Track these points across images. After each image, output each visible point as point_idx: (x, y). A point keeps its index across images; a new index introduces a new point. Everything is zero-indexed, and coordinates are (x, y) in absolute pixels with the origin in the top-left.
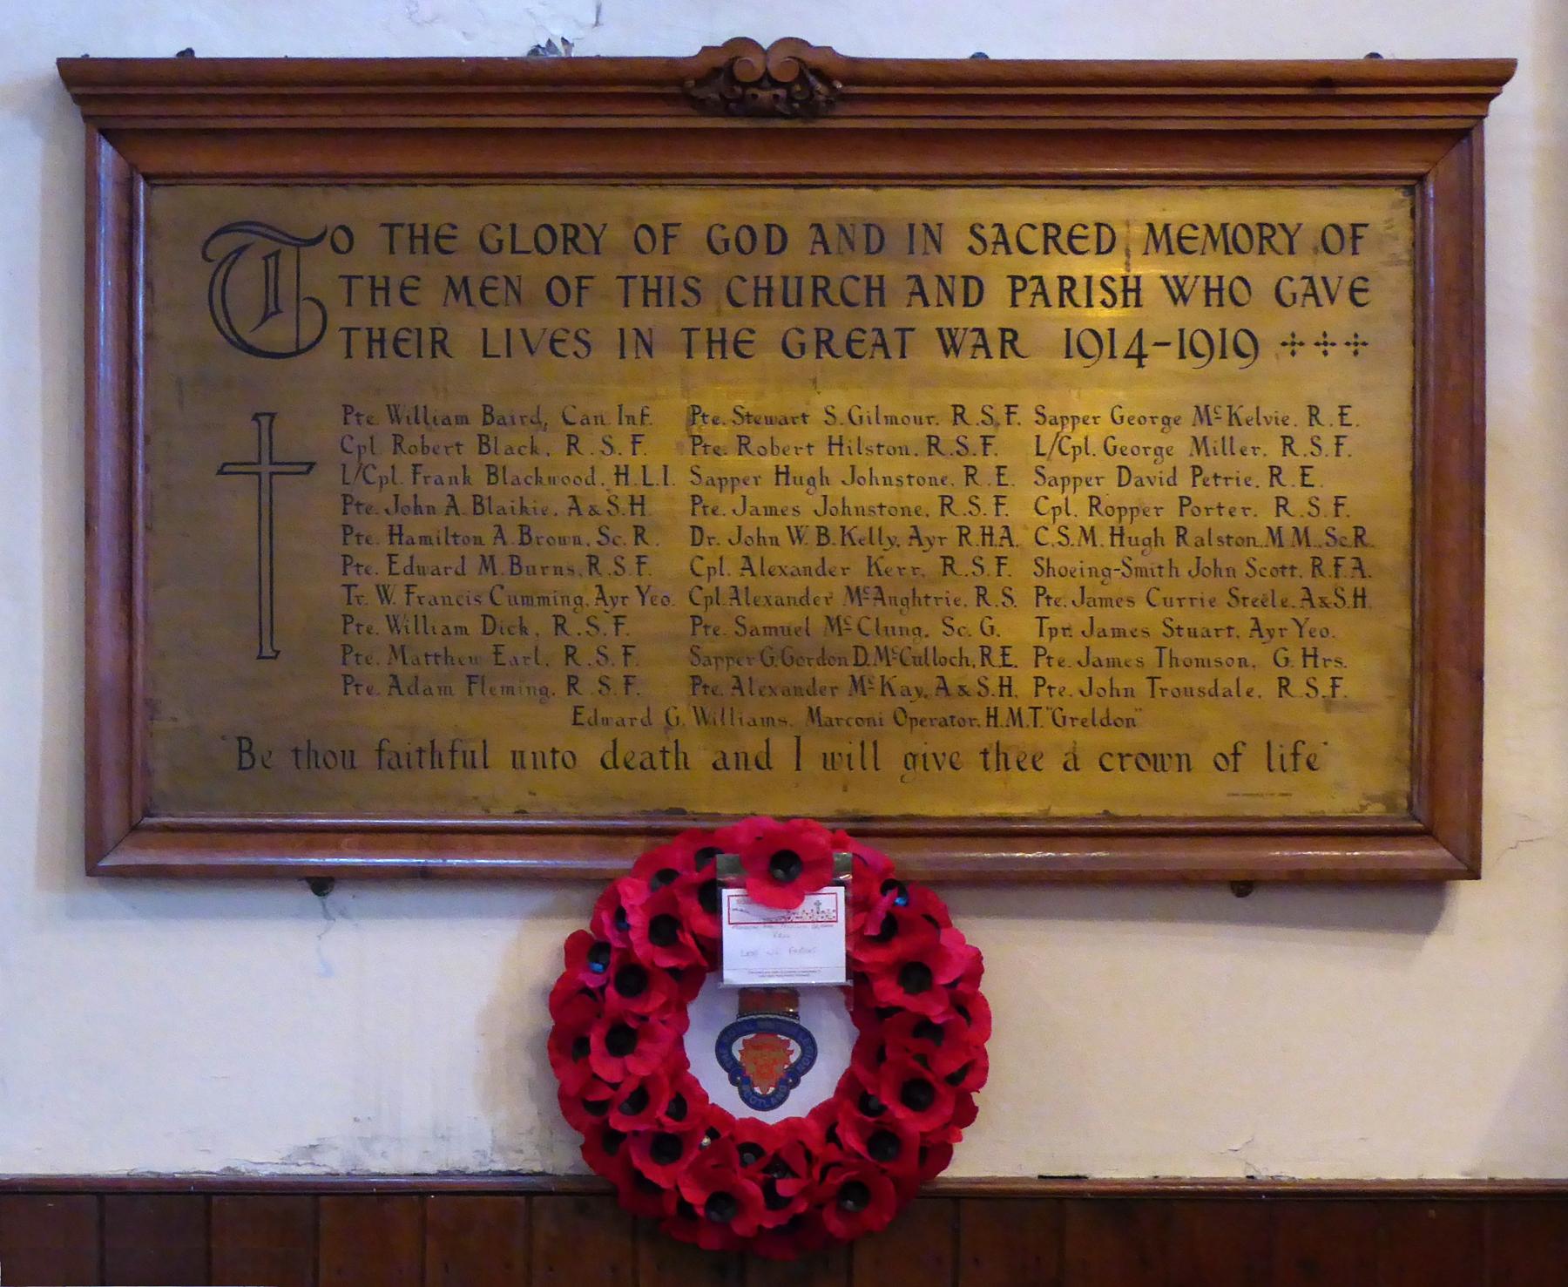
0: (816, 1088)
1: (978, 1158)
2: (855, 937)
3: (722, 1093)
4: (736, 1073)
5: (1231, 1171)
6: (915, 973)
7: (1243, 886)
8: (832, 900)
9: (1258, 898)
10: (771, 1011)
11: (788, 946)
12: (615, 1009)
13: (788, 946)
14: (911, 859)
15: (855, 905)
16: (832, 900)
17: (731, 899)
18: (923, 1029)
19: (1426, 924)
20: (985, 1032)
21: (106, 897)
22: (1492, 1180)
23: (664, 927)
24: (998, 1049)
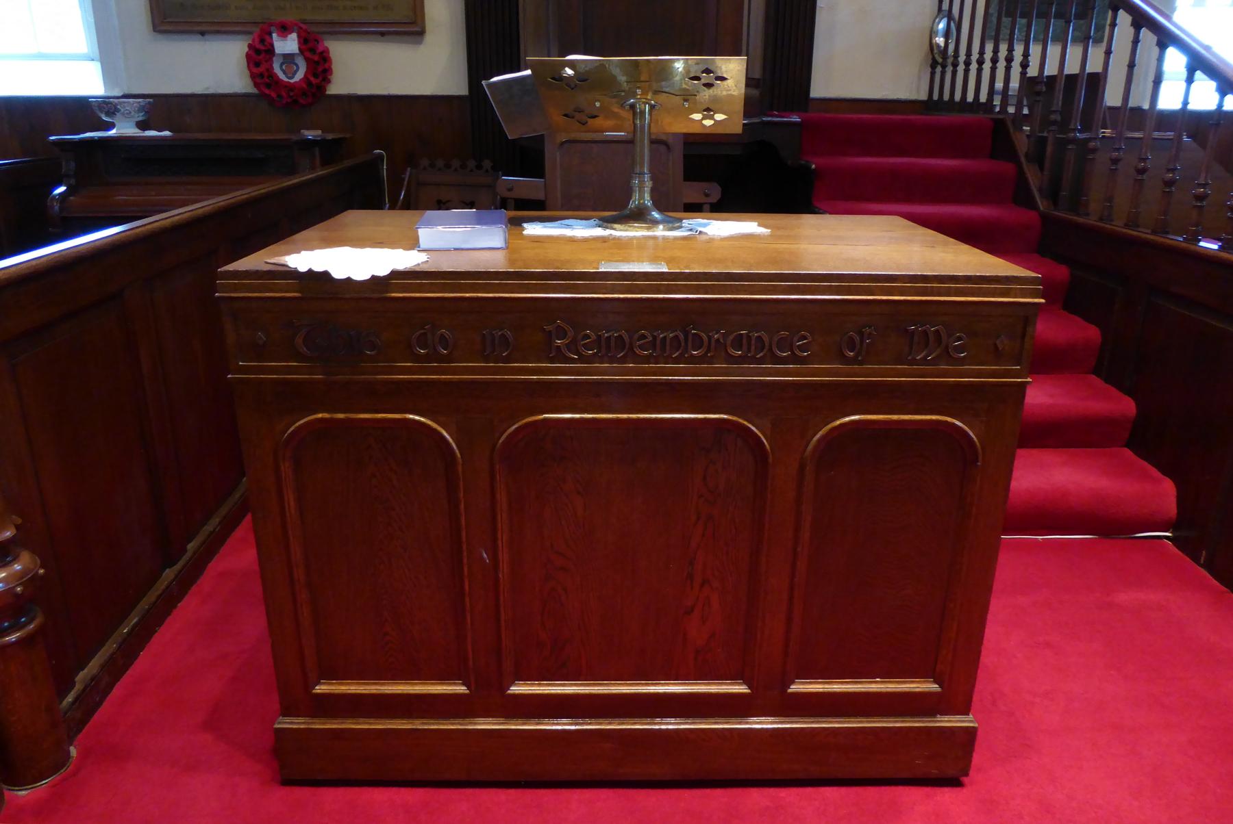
0: (299, 76)
1: (334, 89)
2: (299, 43)
3: (282, 76)
4: (284, 73)
5: (385, 93)
6: (313, 50)
7: (383, 34)
8: (294, 36)
9: (386, 37)
10: (288, 58)
11: (287, 45)
12: (259, 57)
13: (287, 45)
14: (314, 29)
15: (299, 37)
16: (294, 36)
17: (274, 35)
18: (320, 66)
19: (420, 43)
20: (405, 249)
21: (160, 36)
22: (1207, 48)
23: (262, 41)
24: (334, 67)
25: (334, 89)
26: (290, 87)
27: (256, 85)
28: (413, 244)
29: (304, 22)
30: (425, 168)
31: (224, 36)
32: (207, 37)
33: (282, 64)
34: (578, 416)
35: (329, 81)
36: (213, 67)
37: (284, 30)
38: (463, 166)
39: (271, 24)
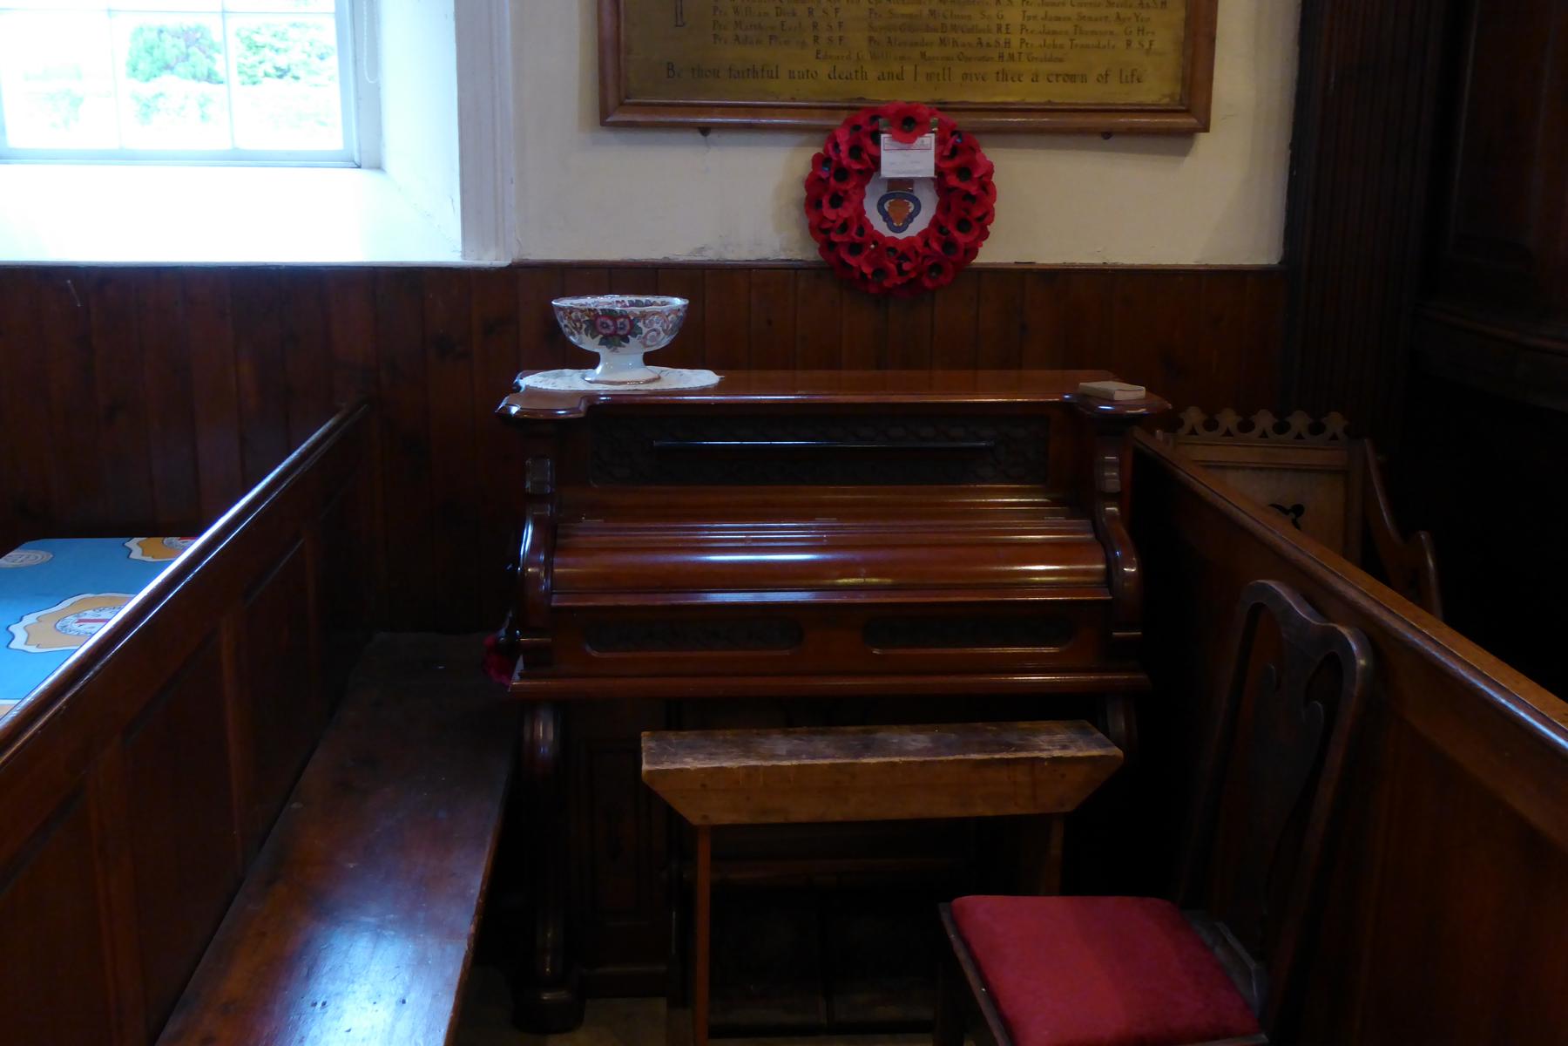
1: (991, 254)
2: (940, 157)
3: (887, 233)
4: (886, 217)
6: (965, 172)
7: (1107, 135)
8: (929, 140)
10: (901, 188)
12: (833, 187)
13: (909, 160)
14: (963, 121)
15: (940, 142)
16: (929, 140)
18: (966, 196)
19: (1184, 152)
23: (856, 150)
24: (999, 206)
25: (991, 254)
26: (902, 251)
27: (827, 246)
28: (747, 753)
29: (943, 107)
30: (1193, 432)
31: (765, 137)
32: (712, 136)
33: (880, 205)
34: (969, 650)
35: (985, 235)
36: (734, 200)
37: (908, 124)
38: (1281, 428)
39: (875, 114)
